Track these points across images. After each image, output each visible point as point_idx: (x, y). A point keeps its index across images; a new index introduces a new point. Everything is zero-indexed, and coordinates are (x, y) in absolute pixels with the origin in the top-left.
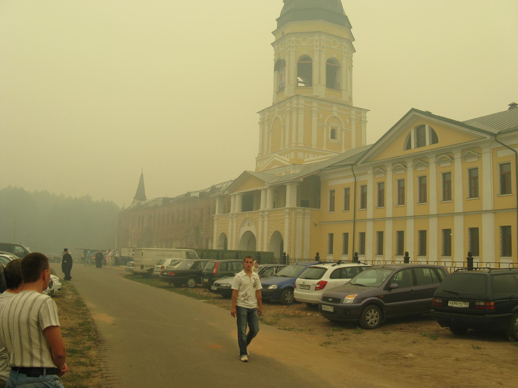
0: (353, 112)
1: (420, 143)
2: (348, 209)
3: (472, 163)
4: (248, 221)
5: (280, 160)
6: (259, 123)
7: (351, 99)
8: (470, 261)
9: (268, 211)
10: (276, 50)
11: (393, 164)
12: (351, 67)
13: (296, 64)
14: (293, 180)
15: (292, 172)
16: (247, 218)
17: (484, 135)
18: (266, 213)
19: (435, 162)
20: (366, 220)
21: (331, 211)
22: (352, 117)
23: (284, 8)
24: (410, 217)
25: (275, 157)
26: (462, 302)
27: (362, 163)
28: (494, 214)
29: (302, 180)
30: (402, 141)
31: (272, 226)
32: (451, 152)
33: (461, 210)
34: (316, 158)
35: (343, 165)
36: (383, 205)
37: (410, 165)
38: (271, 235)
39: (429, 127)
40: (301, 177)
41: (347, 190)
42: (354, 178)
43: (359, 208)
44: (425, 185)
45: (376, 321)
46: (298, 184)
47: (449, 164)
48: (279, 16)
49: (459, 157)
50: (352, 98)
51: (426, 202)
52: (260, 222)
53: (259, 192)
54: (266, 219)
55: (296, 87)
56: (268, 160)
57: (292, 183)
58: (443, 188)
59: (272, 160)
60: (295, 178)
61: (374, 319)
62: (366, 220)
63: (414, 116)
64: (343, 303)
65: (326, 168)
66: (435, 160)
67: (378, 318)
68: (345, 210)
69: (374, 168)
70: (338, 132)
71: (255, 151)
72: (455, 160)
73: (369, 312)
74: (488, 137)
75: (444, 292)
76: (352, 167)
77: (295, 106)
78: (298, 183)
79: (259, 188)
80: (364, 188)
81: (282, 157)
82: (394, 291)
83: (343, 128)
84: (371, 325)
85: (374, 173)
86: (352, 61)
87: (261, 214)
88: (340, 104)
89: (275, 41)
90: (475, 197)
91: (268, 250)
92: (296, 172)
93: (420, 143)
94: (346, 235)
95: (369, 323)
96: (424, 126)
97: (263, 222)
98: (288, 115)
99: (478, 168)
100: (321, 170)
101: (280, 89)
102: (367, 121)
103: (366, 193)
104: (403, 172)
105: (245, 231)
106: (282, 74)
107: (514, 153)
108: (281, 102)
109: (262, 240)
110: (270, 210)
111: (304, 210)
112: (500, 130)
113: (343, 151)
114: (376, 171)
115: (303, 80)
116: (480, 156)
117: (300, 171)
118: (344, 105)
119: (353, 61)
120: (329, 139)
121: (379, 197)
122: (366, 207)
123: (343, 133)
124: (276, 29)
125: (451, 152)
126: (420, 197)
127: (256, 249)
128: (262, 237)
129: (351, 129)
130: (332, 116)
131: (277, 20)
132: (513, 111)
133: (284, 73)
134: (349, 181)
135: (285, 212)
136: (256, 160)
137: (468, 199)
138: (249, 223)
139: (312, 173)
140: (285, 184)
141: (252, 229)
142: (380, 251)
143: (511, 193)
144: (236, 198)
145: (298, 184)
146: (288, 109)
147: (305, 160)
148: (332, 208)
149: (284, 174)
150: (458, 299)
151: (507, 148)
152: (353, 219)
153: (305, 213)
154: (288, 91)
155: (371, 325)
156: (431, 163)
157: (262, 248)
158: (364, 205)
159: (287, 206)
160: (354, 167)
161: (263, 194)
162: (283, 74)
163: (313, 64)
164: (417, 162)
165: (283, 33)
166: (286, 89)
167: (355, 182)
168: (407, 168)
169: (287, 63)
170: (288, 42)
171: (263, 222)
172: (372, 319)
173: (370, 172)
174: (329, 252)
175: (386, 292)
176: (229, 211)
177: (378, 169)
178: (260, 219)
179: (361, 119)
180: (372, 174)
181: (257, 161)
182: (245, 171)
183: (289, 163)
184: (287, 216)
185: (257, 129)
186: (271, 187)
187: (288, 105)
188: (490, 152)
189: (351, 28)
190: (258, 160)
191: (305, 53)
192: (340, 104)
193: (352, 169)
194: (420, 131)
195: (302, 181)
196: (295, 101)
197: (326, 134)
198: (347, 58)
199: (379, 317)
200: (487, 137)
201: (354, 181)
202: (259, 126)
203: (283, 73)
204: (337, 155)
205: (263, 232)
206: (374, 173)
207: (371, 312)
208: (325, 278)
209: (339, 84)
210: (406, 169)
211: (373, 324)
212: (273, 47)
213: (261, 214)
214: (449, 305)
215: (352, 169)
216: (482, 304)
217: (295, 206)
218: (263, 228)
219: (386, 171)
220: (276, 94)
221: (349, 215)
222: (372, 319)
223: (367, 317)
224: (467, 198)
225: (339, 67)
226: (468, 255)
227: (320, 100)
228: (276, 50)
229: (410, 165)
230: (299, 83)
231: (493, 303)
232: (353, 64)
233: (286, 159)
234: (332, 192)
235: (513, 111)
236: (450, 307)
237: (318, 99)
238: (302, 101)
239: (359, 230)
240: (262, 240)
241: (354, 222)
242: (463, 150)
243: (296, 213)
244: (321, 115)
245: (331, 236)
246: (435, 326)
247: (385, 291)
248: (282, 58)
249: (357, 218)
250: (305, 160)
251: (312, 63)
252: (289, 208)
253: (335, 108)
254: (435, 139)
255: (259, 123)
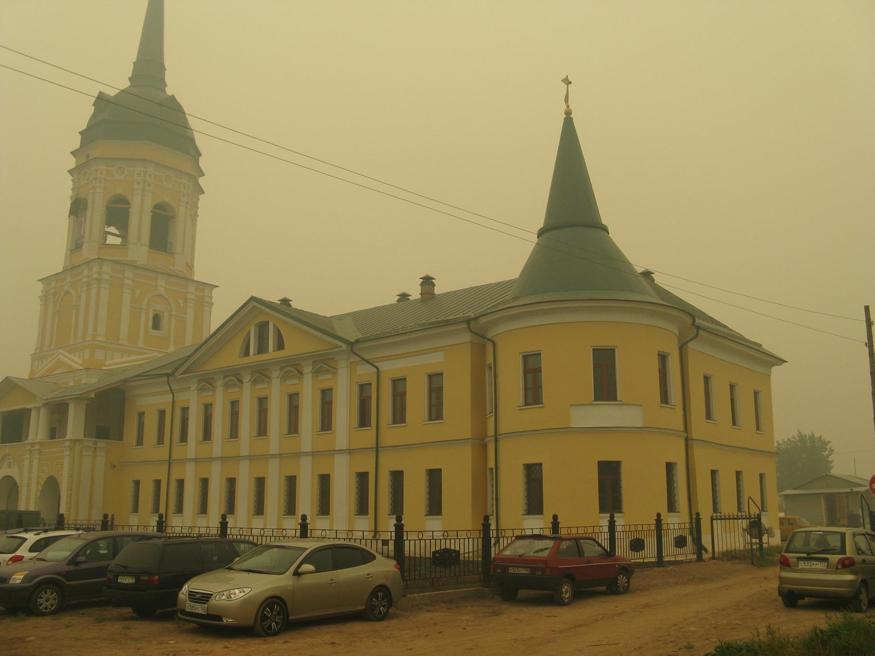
0: (191, 288)
1: (262, 348)
2: (163, 443)
3: (325, 380)
4: (9, 459)
5: (66, 359)
6: (40, 297)
7: (190, 267)
8: (224, 525)
9: (39, 443)
10: (76, 182)
11: (225, 377)
12: (194, 217)
13: (104, 208)
14: (79, 396)
15: (84, 381)
16: (8, 455)
17: (339, 343)
18: (37, 447)
19: (278, 377)
20: (184, 461)
21: (325, 431)
22: (189, 296)
23: (94, 116)
24: (274, 456)
25: (60, 356)
26: (130, 577)
27: (182, 374)
28: (349, 455)
29: (92, 396)
30: (237, 345)
31: (45, 468)
32: (300, 364)
33: (193, 457)
34: (126, 359)
35: (157, 375)
36: (236, 437)
37: (307, 369)
38: (43, 483)
39: (275, 326)
40: (90, 391)
41: (162, 413)
42: (171, 395)
43: (178, 440)
44: (266, 410)
45: (52, 606)
46: (88, 402)
47: (296, 381)
48: (85, 128)
49: (309, 371)
50: (193, 266)
51: (331, 430)
52: (27, 462)
53: (28, 412)
54: (36, 456)
55: (102, 244)
56: (49, 359)
57: (77, 399)
58: (289, 415)
59: (56, 359)
60: (80, 393)
61: (49, 602)
62: (184, 461)
63: (254, 307)
64: (8, 583)
65: (130, 379)
66: (279, 374)
67: (57, 601)
68: (289, 434)
69: (200, 381)
70: (165, 319)
71: (31, 343)
72: (305, 375)
73: (42, 594)
74: (344, 346)
75: (117, 566)
76: (168, 378)
77: (96, 276)
78: (87, 399)
79: (28, 406)
80: (185, 410)
81: (71, 356)
82: (83, 566)
83: (173, 313)
84: (45, 611)
85: (313, 371)
86: (197, 208)
87: (28, 447)
88: (169, 275)
89: (75, 168)
90: (401, 422)
91: (37, 507)
92: (92, 381)
93: (262, 348)
94: (158, 483)
95: (42, 608)
96: (267, 323)
97: (31, 462)
98: (84, 289)
99: (442, 374)
100: (125, 381)
101: (76, 246)
102: (213, 304)
103: (187, 419)
104: (237, 389)
105: (2, 476)
106: (81, 222)
107: (376, 370)
108: (76, 267)
109: (29, 492)
110: (42, 443)
111: (95, 443)
112: (454, 316)
113: (172, 349)
114: (202, 386)
115: (119, 232)
116: (335, 371)
117: (97, 380)
118: (176, 276)
119: (198, 208)
120: (149, 330)
121: (204, 428)
122: (186, 441)
123: (173, 321)
124: (78, 146)
125: (300, 364)
126: (429, 411)
127: (18, 505)
128: (29, 485)
129: (186, 314)
130: (156, 294)
131: (81, 133)
132: (406, 303)
133: (85, 220)
134: (163, 400)
135: (66, 445)
136: (32, 358)
137: (427, 423)
138: (10, 462)
139: (113, 384)
140: (67, 402)
141: (14, 472)
142: (259, 509)
143: (442, 419)
144: (41, 413)
145: (88, 402)
146: (85, 280)
147: (106, 363)
148: (140, 442)
149: (71, 384)
150: (127, 573)
151: (366, 363)
152: (168, 459)
153: (96, 447)
154: (88, 251)
155: (45, 611)
156: (307, 373)
157: (28, 504)
158: (184, 438)
159: (69, 435)
160: (170, 378)
161: (33, 414)
162: (83, 222)
163: (130, 210)
164: (319, 366)
165: (88, 156)
166: (85, 246)
167: (173, 401)
168: (303, 375)
169: (90, 205)
170: (94, 172)
171: (31, 462)
172: (47, 603)
173: (194, 386)
174: (200, 510)
175: (72, 568)
176: (63, 434)
177: (204, 383)
178: (27, 456)
179: (204, 299)
180: (196, 391)
181: (33, 359)
182: (7, 378)
183: (80, 365)
184: (68, 453)
185: (35, 307)
186: (45, 405)
187: (86, 272)
188: (347, 367)
189: (200, 155)
190: (35, 358)
191: (119, 191)
192: (169, 275)
193: (168, 382)
194: (262, 328)
195: (94, 398)
196: (96, 269)
197: (145, 321)
198: (187, 203)
199: (57, 600)
200: (343, 346)
201: (172, 400)
202: (40, 302)
203: (83, 220)
204: (160, 355)
205: (30, 478)
206: (200, 389)
207: (46, 594)
208: (23, 551)
209: (172, 243)
210: (242, 385)
211: (48, 608)
212: (71, 175)
213: (28, 447)
214: (119, 581)
215: (168, 382)
216: (146, 578)
217: (81, 436)
218: (30, 472)
219: (216, 387)
220: (69, 252)
221: (162, 453)
222: (47, 602)
223: (39, 600)
224: (226, 439)
225: (173, 217)
226: (104, 518)
227: (137, 267)
228: (76, 182)
229: (307, 369)
230: (109, 237)
231: (157, 577)
232: (199, 212)
233: (76, 359)
234: (141, 415)
235: (406, 303)
236: (120, 583)
237: (133, 266)
238: (107, 269)
239: (176, 475)
240: (29, 492)
241: (170, 463)
242: (314, 362)
243: (82, 448)
244: (138, 292)
245: (137, 483)
246: (128, 611)
247: (68, 566)
248: (83, 196)
249: (174, 457)
250: (106, 363)
251: (129, 208)
252: (71, 440)
253: (161, 282)
254: (280, 345)
255: (40, 297)
